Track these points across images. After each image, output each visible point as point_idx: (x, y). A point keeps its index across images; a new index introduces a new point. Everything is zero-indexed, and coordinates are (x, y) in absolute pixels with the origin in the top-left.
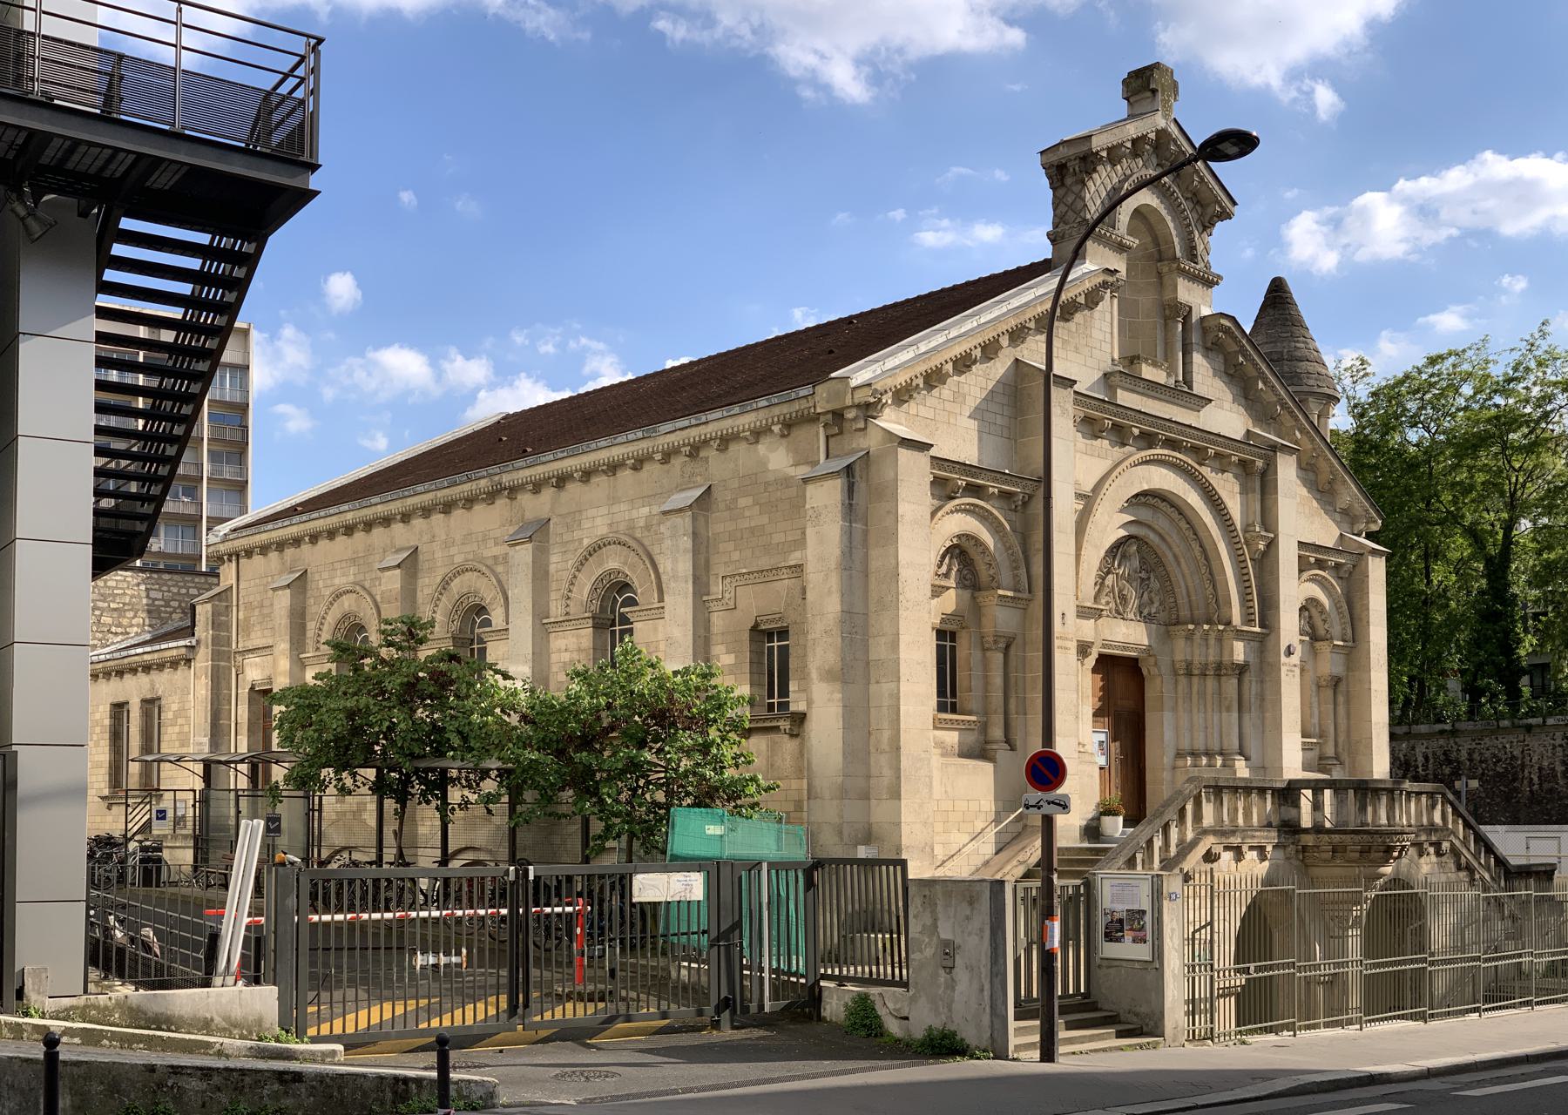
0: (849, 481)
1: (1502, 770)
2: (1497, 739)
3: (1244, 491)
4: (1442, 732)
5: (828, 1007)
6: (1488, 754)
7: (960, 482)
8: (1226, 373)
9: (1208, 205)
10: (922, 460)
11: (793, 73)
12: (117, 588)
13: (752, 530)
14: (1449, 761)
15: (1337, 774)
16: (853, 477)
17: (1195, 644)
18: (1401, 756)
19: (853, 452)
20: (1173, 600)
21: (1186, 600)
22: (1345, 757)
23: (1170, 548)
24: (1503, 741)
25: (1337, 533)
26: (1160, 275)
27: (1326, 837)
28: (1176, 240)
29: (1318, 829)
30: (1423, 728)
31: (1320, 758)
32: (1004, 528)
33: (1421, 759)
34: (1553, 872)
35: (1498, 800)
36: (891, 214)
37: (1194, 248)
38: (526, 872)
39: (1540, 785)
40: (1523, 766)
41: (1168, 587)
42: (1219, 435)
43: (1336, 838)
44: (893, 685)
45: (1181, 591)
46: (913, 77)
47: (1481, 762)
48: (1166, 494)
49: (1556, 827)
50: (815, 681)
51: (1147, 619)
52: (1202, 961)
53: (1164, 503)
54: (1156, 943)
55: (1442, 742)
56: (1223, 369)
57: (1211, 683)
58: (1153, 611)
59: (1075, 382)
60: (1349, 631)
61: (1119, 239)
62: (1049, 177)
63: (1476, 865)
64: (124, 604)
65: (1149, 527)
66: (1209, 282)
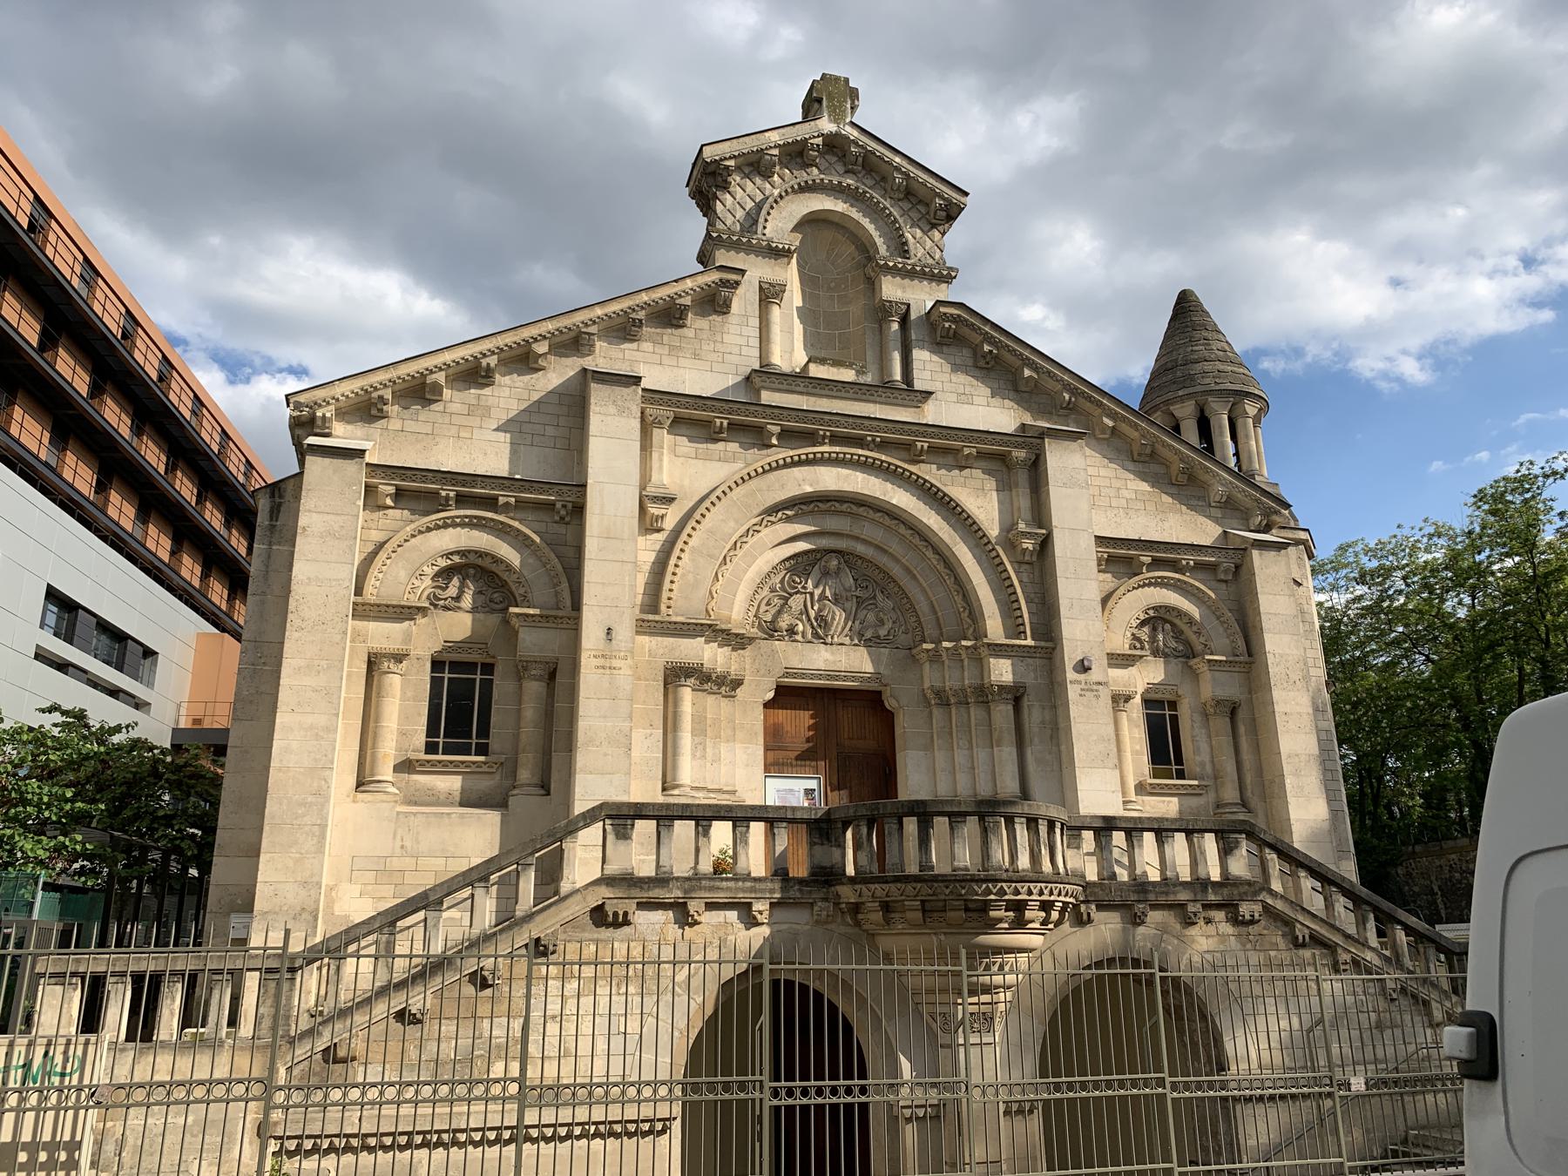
3: (1004, 487)
11: (1368, 374)
17: (946, 667)
20: (913, 619)
22: (1254, 801)
23: (897, 560)
25: (1219, 530)
27: (909, 888)
28: (879, 241)
32: (533, 541)
36: (1478, 456)
37: (905, 243)
41: (905, 605)
45: (923, 607)
46: (1470, 358)
51: (871, 643)
53: (862, 509)
56: (970, 362)
57: (976, 713)
58: (882, 632)
59: (640, 378)
60: (1241, 643)
65: (857, 538)
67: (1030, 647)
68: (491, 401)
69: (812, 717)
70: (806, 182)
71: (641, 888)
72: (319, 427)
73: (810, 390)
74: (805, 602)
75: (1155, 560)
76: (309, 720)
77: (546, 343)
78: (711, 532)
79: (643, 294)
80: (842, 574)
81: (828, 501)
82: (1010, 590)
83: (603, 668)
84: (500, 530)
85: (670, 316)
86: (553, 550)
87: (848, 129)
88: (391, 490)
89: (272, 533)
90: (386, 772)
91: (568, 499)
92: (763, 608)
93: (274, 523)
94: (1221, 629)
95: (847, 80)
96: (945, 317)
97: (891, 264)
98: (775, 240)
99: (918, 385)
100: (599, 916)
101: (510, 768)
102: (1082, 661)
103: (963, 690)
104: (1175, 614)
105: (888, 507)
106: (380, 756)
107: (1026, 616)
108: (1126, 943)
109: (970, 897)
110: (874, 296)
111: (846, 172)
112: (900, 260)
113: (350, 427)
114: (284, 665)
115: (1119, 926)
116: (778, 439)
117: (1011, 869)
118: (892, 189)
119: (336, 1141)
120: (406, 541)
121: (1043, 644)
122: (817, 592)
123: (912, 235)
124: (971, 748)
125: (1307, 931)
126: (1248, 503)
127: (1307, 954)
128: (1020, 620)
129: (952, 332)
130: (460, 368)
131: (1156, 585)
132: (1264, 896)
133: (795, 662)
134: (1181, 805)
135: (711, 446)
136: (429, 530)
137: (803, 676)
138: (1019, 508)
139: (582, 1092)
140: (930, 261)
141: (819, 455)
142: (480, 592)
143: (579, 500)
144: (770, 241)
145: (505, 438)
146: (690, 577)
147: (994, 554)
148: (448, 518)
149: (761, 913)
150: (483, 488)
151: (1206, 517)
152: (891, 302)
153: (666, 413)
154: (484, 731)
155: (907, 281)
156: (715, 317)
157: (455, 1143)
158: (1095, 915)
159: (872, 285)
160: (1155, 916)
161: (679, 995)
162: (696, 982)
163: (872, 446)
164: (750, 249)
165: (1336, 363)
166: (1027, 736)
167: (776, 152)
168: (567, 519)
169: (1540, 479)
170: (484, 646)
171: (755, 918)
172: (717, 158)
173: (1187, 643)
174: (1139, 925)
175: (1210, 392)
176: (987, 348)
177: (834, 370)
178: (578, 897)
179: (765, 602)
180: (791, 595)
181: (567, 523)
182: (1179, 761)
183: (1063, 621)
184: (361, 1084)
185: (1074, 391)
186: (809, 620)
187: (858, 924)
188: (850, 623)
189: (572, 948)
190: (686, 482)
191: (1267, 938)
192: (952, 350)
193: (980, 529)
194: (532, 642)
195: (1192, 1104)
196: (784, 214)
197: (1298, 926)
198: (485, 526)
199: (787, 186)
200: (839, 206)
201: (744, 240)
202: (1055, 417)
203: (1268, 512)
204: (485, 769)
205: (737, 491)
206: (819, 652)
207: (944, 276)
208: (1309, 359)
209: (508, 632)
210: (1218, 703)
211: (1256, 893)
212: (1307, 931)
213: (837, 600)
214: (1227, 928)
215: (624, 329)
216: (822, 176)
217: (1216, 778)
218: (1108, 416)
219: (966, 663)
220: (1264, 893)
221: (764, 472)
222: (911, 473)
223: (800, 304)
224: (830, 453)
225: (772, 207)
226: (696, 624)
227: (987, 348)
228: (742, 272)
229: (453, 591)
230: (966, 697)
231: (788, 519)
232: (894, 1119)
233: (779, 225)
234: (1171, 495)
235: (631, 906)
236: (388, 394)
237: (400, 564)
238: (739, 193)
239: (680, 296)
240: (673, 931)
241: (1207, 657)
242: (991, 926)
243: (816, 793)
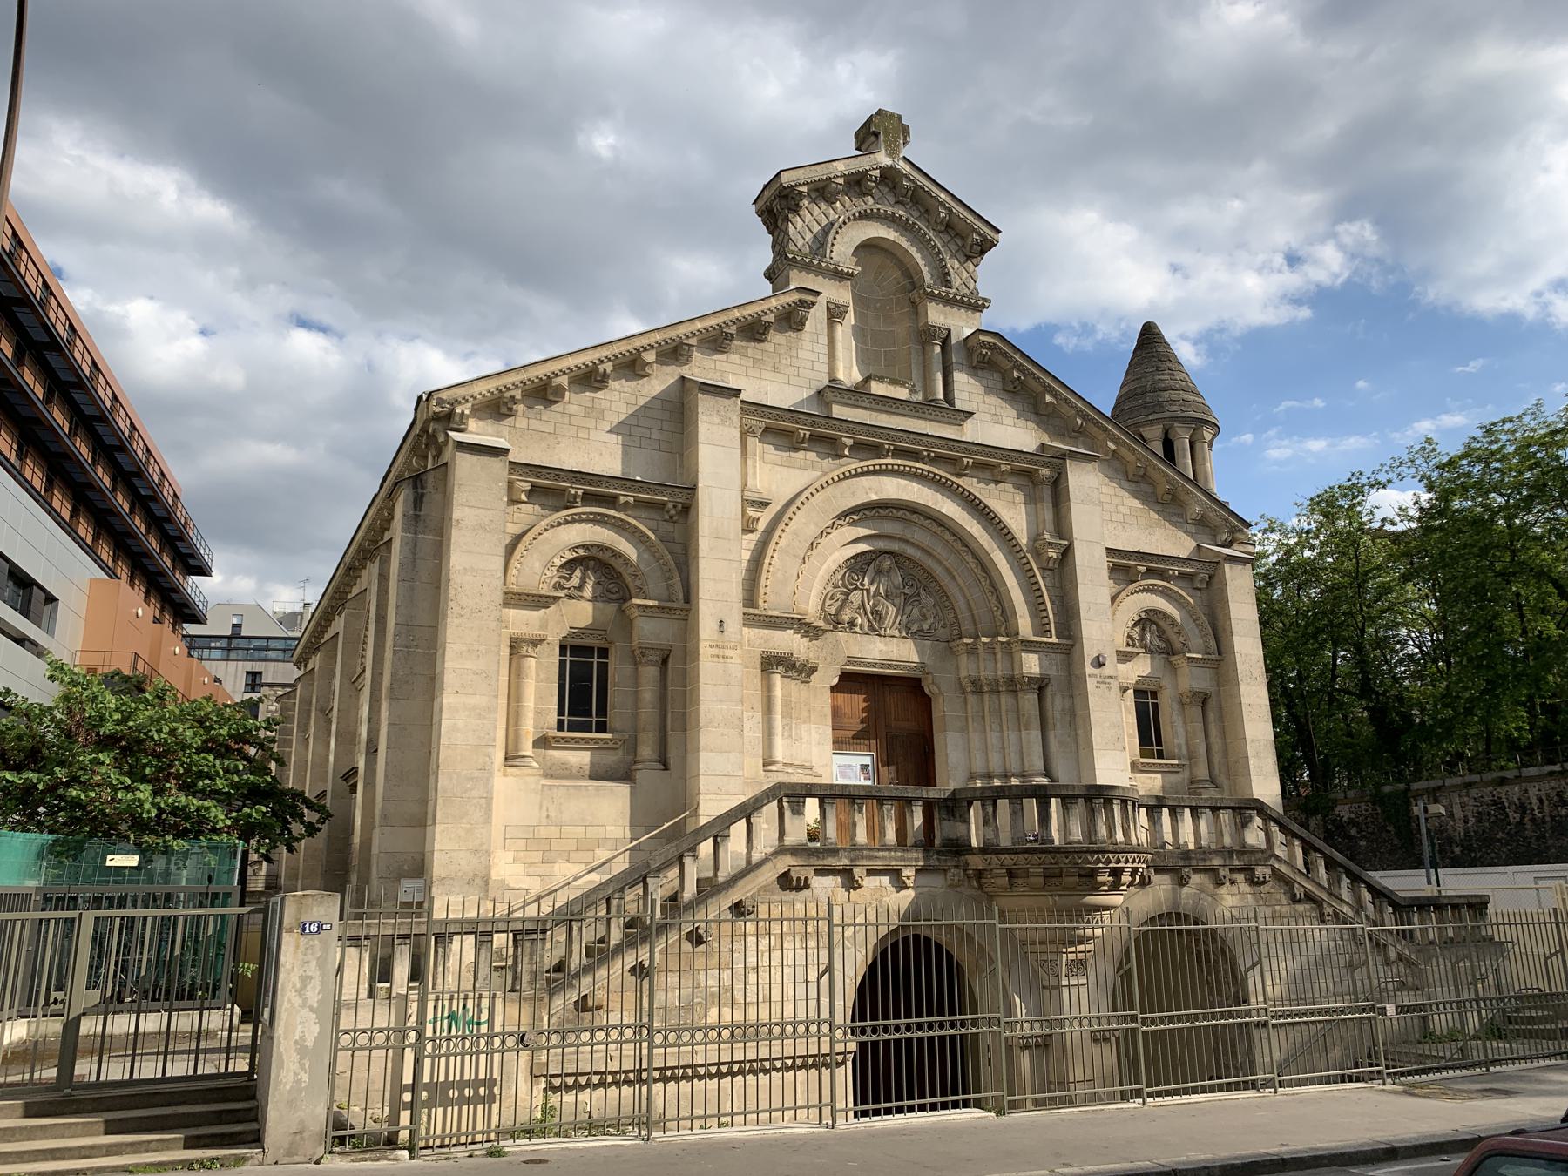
3: (1031, 500)
4: (1551, 773)
8: (1004, 390)
9: (968, 236)
10: (497, 466)
15: (1209, 794)
20: (953, 615)
21: (967, 614)
22: (1222, 779)
23: (940, 563)
25: (1194, 544)
26: (914, 304)
28: (925, 270)
29: (988, 849)
30: (1533, 771)
31: (1192, 782)
32: (648, 537)
33: (1535, 801)
36: (1243, 437)
37: (948, 274)
41: (944, 600)
43: (1008, 859)
45: (960, 604)
46: (1239, 347)
48: (918, 507)
51: (917, 635)
53: (915, 516)
55: (1553, 783)
56: (999, 386)
57: (1006, 700)
58: (926, 627)
60: (1213, 643)
65: (907, 541)
67: (1054, 644)
68: (604, 404)
69: (865, 701)
70: (872, 210)
71: (818, 857)
72: (456, 423)
73: (873, 406)
74: (863, 597)
75: (1149, 569)
76: (472, 701)
77: (654, 352)
78: (796, 534)
79: (736, 310)
80: (892, 574)
81: (887, 508)
82: (1038, 593)
83: (718, 656)
84: (619, 526)
85: (754, 330)
86: (666, 547)
87: (902, 163)
88: (527, 486)
89: (417, 522)
90: (527, 749)
91: (678, 500)
92: (828, 602)
93: (418, 513)
94: (1197, 631)
95: (899, 117)
96: (983, 344)
97: (936, 292)
98: (841, 264)
99: (959, 405)
100: (786, 882)
101: (632, 745)
102: (1098, 657)
103: (996, 680)
104: (1161, 616)
105: (937, 515)
106: (523, 733)
107: (1051, 616)
108: (1175, 903)
109: (1084, 866)
110: (917, 319)
111: (896, 203)
112: (944, 289)
113: (481, 423)
114: (447, 649)
115: (1170, 887)
116: (849, 451)
117: (1109, 842)
118: (936, 222)
119: (755, 1064)
120: (540, 534)
121: (1064, 641)
122: (873, 589)
123: (952, 264)
124: (1002, 731)
125: (1302, 890)
126: (1218, 521)
127: (1300, 908)
128: (1046, 620)
129: (987, 358)
130: (580, 372)
131: (1148, 591)
132: (1272, 861)
133: (856, 652)
134: (1164, 781)
135: (793, 455)
136: (559, 524)
137: (862, 664)
138: (1044, 520)
139: (776, 1030)
140: (966, 291)
141: (884, 467)
142: (599, 583)
143: (688, 501)
144: (836, 265)
145: (616, 440)
146: (779, 575)
147: (1025, 560)
148: (575, 514)
149: (908, 878)
150: (607, 487)
151: (1185, 532)
152: (935, 327)
153: (758, 423)
154: (602, 710)
155: (948, 308)
156: (790, 333)
157: (685, 1077)
158: (1154, 878)
159: (916, 309)
160: (1196, 879)
161: (849, 948)
162: (860, 937)
163: (926, 459)
164: (819, 271)
165: (1122, 343)
166: (1050, 721)
167: (841, 181)
168: (675, 518)
169: (1367, 487)
170: (603, 633)
171: (904, 882)
172: (793, 184)
173: (1168, 641)
174: (1184, 885)
175: (1176, 419)
176: (1016, 374)
177: (891, 387)
178: (769, 865)
179: (829, 596)
180: (851, 591)
181: (675, 522)
182: (1159, 743)
183: (1083, 622)
184: (500, 1033)
185: (1085, 417)
186: (866, 614)
187: (981, 887)
188: (899, 618)
189: (763, 909)
190: (774, 487)
191: (1273, 896)
192: (985, 373)
193: (1014, 538)
194: (649, 630)
195: (1217, 1031)
196: (845, 240)
197: (1296, 885)
198: (606, 522)
199: (849, 214)
200: (890, 234)
201: (816, 262)
202: (1067, 439)
203: (1233, 531)
204: (611, 745)
205: (817, 495)
206: (875, 643)
207: (976, 305)
208: (1099, 336)
209: (625, 622)
210: (1195, 694)
211: (1267, 859)
212: (1302, 890)
213: (887, 597)
214: (1245, 888)
215: (717, 341)
216: (879, 206)
217: (1190, 758)
218: (1112, 441)
219: (999, 656)
220: (1273, 859)
221: (840, 480)
222: (959, 486)
223: (853, 323)
224: (893, 465)
225: (837, 233)
226: (788, 618)
227: (1016, 374)
228: (818, 293)
229: (575, 581)
230: (997, 685)
231: (854, 523)
232: (1009, 1048)
233: (842, 250)
234: (1157, 512)
235: (811, 871)
236: (518, 394)
237: (535, 556)
238: (808, 217)
239: (766, 313)
240: (841, 894)
241: (1188, 655)
242: (1095, 889)
243: (870, 768)
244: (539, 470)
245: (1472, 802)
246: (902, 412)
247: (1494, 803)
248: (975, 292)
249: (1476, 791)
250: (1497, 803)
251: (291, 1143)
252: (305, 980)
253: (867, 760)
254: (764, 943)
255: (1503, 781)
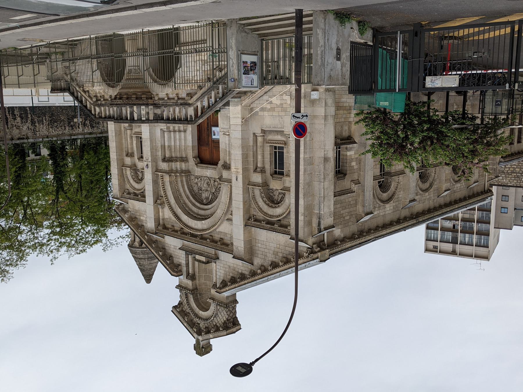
0: (320, 227)
1: (55, 123)
2: (57, 134)
5: (371, 34)
6: (60, 129)
7: (277, 226)
12: (513, 180)
13: (345, 208)
14: (71, 126)
16: (318, 228)
18: (87, 128)
19: (316, 237)
24: (55, 133)
31: (132, 129)
33: (80, 127)
34: (51, 90)
35: (56, 114)
38: (510, 87)
39: (43, 119)
40: (48, 125)
42: (177, 238)
44: (306, 157)
47: (62, 126)
49: (40, 105)
50: (332, 157)
52: (217, 55)
54: (239, 61)
55: (74, 132)
59: (233, 258)
61: (215, 302)
62: (238, 321)
63: (82, 93)
64: (511, 175)
66: (179, 287)
68: (273, 256)
72: (309, 251)
84: (267, 214)
127: (87, 89)
176: (168, 262)
189: (196, 88)
200: (197, 310)
244: (284, 233)
245: (100, 127)
246: (196, 250)
247: (93, 127)
248: (181, 291)
249: (99, 131)
250: (92, 127)
251: (232, 24)
252: (233, 66)
253: (214, 137)
254: (196, 78)
255: (90, 133)
